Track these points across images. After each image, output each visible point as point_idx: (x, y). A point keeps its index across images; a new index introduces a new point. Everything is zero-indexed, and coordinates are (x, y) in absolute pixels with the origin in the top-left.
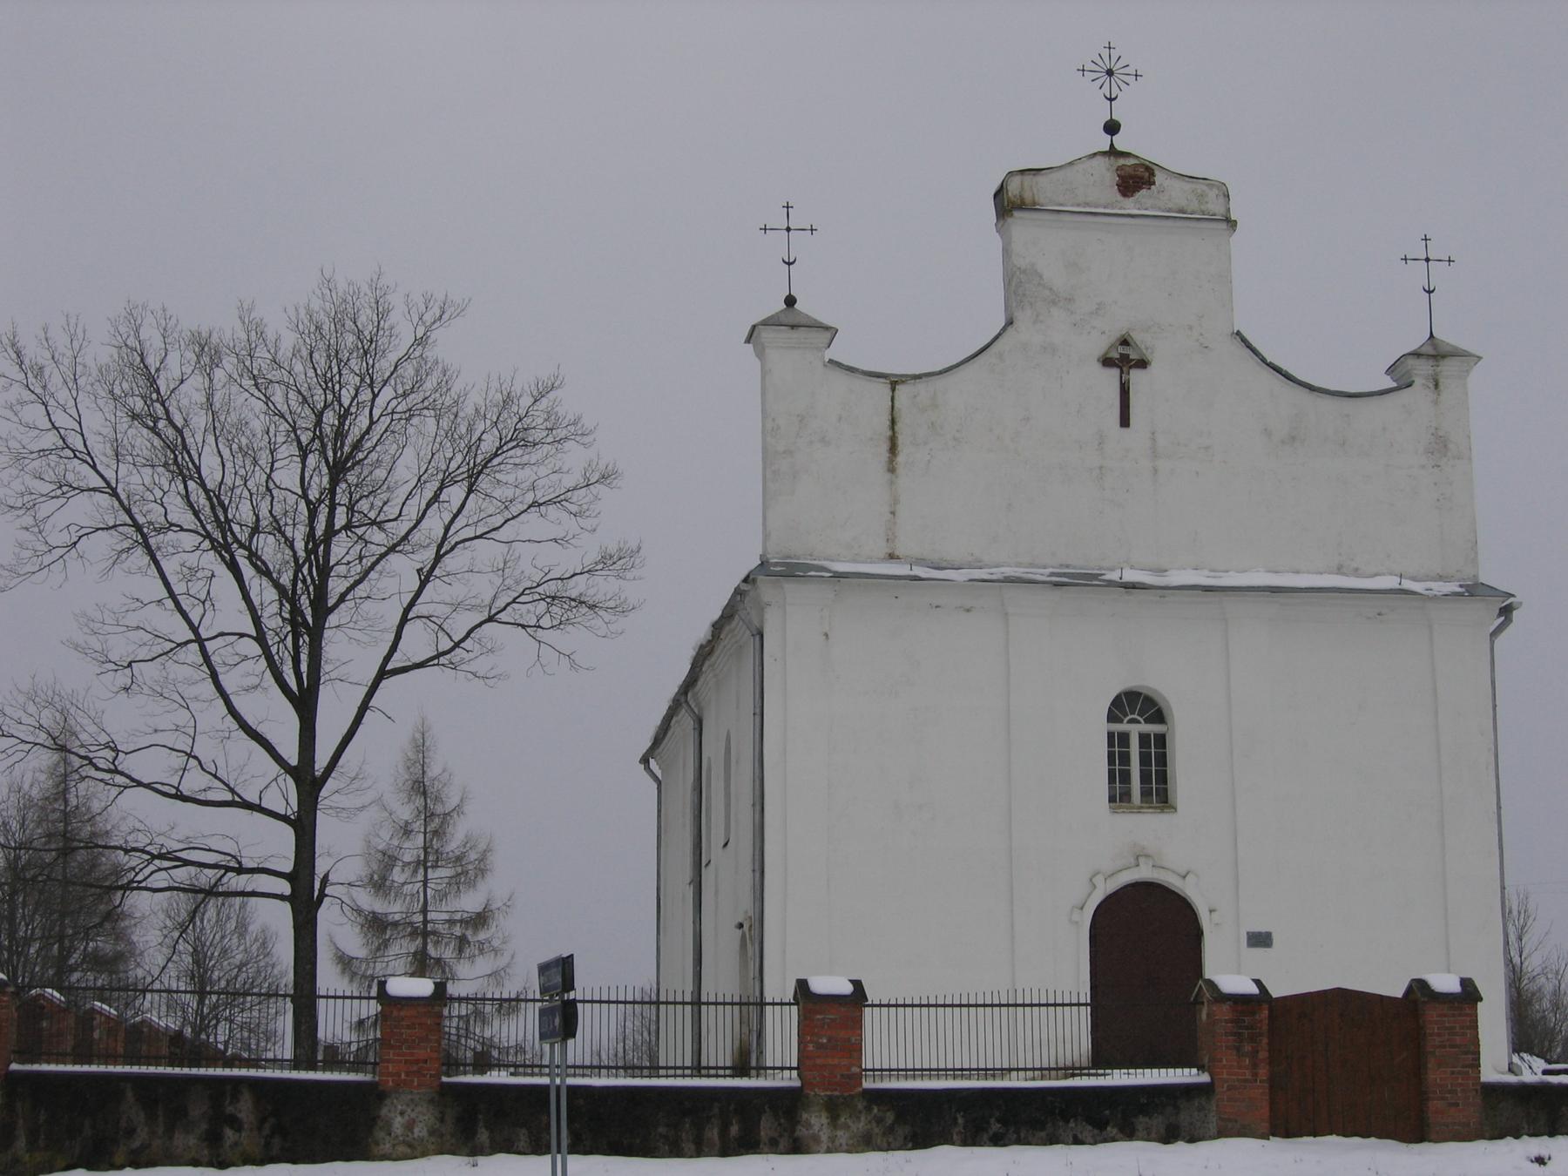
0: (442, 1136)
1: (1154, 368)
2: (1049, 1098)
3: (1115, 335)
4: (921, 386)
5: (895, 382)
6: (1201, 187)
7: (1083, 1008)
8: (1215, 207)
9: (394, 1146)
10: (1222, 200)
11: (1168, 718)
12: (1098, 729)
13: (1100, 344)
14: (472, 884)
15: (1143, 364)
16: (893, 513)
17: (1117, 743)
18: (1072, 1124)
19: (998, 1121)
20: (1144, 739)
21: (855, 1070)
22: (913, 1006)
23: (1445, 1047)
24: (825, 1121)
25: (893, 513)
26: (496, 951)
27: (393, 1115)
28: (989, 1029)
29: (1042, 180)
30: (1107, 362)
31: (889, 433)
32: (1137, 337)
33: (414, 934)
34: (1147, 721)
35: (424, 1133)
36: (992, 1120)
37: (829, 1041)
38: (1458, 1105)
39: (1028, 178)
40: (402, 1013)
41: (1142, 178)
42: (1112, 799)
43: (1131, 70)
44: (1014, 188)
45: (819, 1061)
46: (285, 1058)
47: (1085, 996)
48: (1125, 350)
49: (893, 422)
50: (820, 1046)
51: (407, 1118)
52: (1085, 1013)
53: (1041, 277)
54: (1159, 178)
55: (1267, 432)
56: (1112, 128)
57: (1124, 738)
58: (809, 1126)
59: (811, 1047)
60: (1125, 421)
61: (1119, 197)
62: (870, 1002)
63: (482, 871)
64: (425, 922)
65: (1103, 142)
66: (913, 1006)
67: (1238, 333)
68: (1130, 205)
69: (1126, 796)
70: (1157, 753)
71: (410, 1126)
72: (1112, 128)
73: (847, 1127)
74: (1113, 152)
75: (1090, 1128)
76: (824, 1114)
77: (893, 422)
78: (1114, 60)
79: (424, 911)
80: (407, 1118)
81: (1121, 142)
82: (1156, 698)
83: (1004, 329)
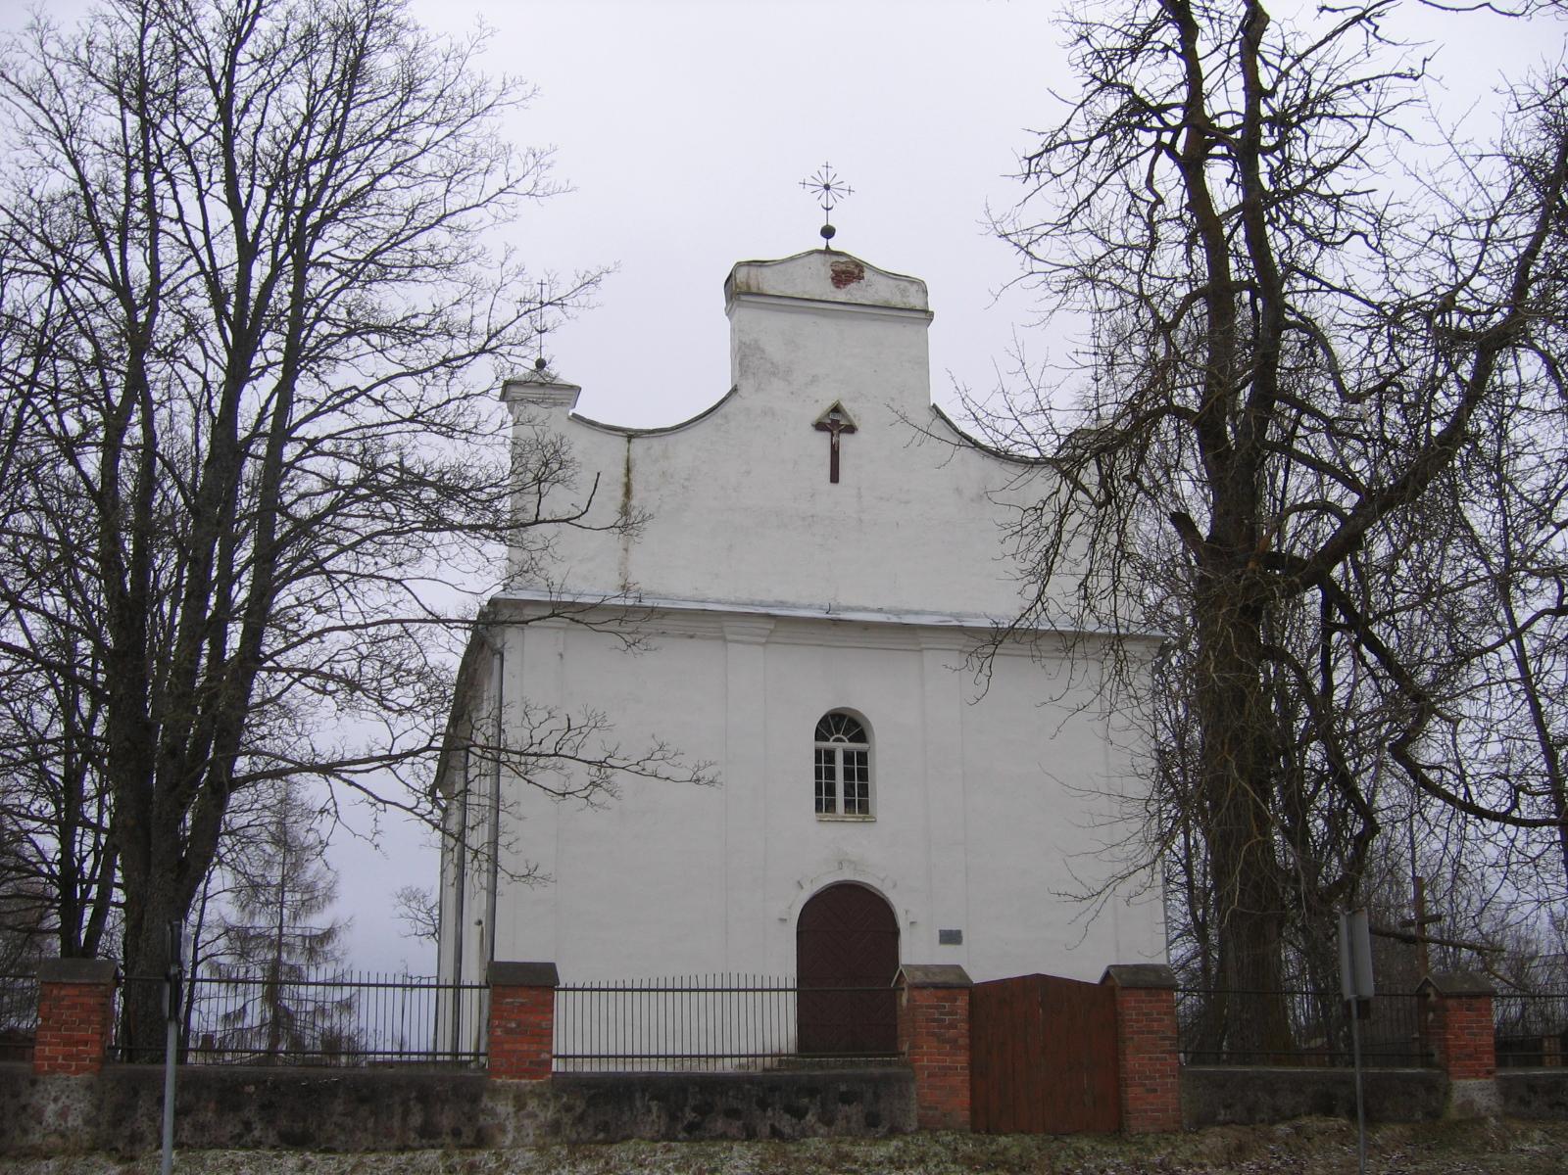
0: (98, 1125)
1: (862, 434)
2: (747, 1086)
3: (828, 404)
4: (656, 443)
5: (631, 435)
6: (903, 284)
7: (789, 993)
8: (915, 301)
9: (44, 1136)
10: (921, 295)
11: (869, 738)
12: (808, 745)
13: (817, 412)
14: (320, 908)
15: (851, 429)
16: (626, 550)
17: (824, 758)
18: (770, 1113)
19: (694, 1109)
20: (848, 757)
21: (545, 1056)
22: (625, 990)
23: (1143, 1033)
24: (511, 1109)
25: (626, 550)
26: (336, 960)
27: (44, 1102)
28: (727, 1019)
29: (766, 271)
30: (820, 426)
31: (625, 480)
32: (846, 406)
33: (271, 945)
34: (851, 740)
35: (80, 1121)
36: (687, 1110)
37: (519, 1025)
38: (1155, 1091)
39: (754, 271)
40: (63, 993)
41: (852, 273)
42: (818, 808)
43: (845, 186)
44: (741, 275)
45: (506, 1046)
46: (440, 1049)
47: (792, 984)
48: (837, 417)
49: (628, 470)
50: (508, 1031)
51: (60, 1104)
52: (792, 997)
53: (763, 351)
54: (867, 274)
55: (958, 491)
56: (828, 232)
57: (830, 755)
58: (493, 1113)
59: (499, 1032)
60: (835, 478)
61: (833, 288)
62: (562, 985)
63: (329, 897)
64: (281, 935)
65: (821, 243)
66: (625, 990)
67: (934, 406)
68: (841, 295)
69: (831, 806)
70: (859, 768)
71: (63, 1114)
72: (828, 232)
73: (533, 1116)
74: (828, 251)
75: (788, 1116)
76: (510, 1103)
77: (628, 470)
78: (831, 176)
79: (281, 928)
80: (60, 1104)
81: (835, 244)
82: (860, 721)
83: (730, 394)
